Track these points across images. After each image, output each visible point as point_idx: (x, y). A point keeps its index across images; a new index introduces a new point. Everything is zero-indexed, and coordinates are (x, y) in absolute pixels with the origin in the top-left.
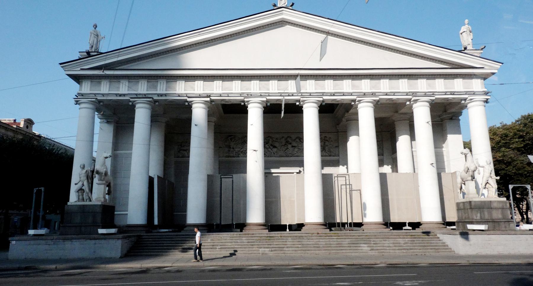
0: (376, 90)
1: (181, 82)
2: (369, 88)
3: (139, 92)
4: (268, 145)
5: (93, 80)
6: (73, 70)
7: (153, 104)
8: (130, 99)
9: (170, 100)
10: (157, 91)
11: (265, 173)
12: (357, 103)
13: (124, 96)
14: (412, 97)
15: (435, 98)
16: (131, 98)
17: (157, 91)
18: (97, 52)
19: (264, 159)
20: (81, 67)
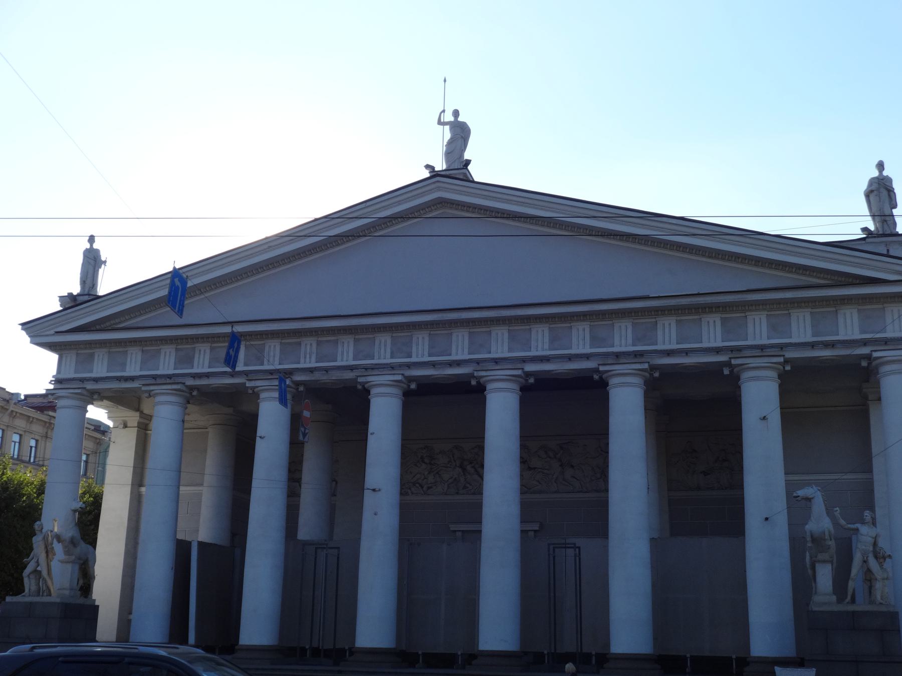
0: (645, 345)
2: (630, 341)
4: (473, 467)
6: (42, 334)
7: (295, 390)
8: (141, 387)
9: (216, 385)
10: (192, 367)
11: (522, 531)
13: (687, 354)
16: (143, 385)
17: (192, 367)
18: (89, 295)
19: (521, 499)
20: (57, 327)
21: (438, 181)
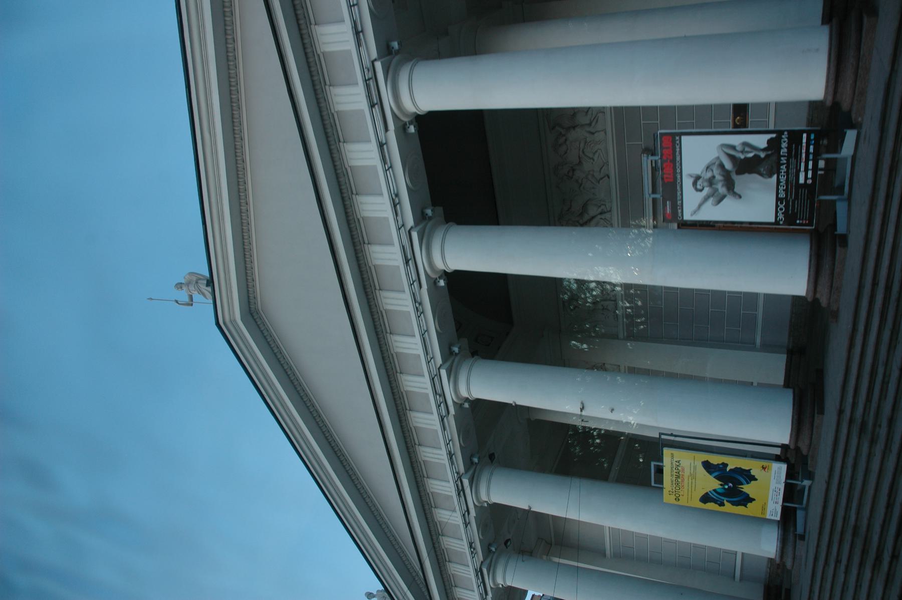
21: (225, 323)
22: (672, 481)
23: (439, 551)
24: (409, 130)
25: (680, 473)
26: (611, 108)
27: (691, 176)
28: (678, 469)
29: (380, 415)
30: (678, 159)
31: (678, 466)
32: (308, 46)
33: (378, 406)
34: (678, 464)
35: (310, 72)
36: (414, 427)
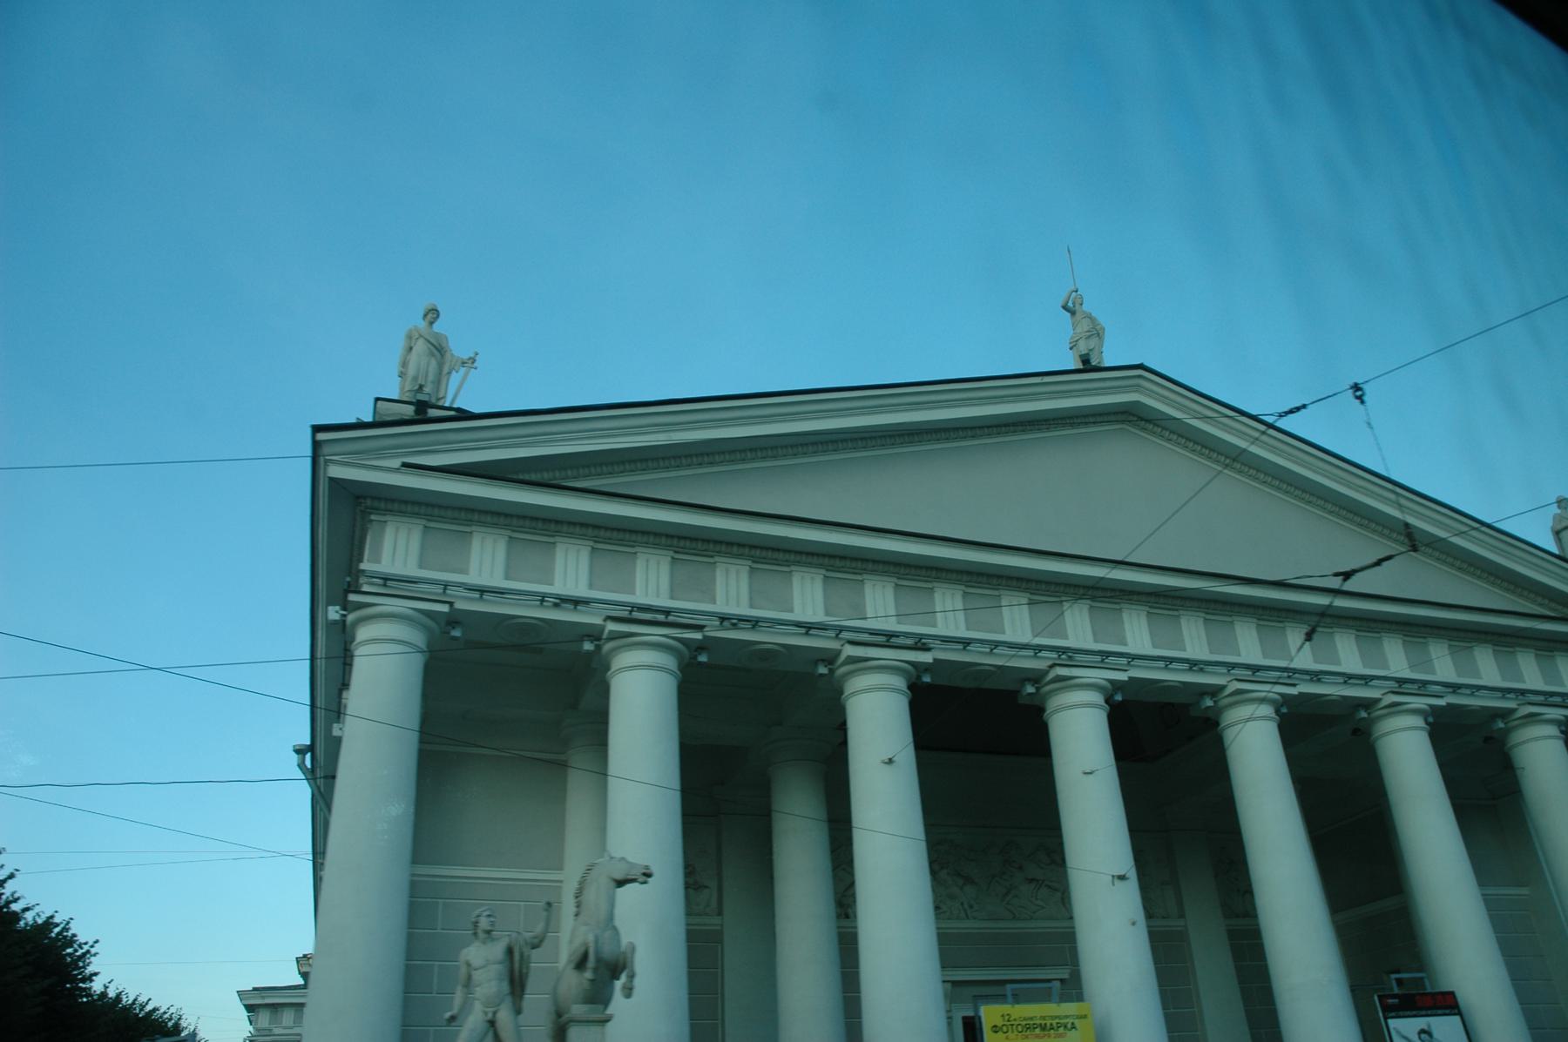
1: (733, 569)
3: (640, 598)
5: (432, 525)
12: (608, 647)
14: (1519, 705)
15: (705, 637)
22: (1031, 1019)
23: (704, 548)
24: (588, 642)
25: (1052, 1031)
26: (1073, 928)
27: (1429, 1026)
28: (1059, 1027)
29: (1059, 558)
30: (1440, 1012)
31: (1066, 1027)
32: (571, 529)
33: (882, 535)
34: (1069, 1026)
35: (550, 521)
36: (385, 522)
